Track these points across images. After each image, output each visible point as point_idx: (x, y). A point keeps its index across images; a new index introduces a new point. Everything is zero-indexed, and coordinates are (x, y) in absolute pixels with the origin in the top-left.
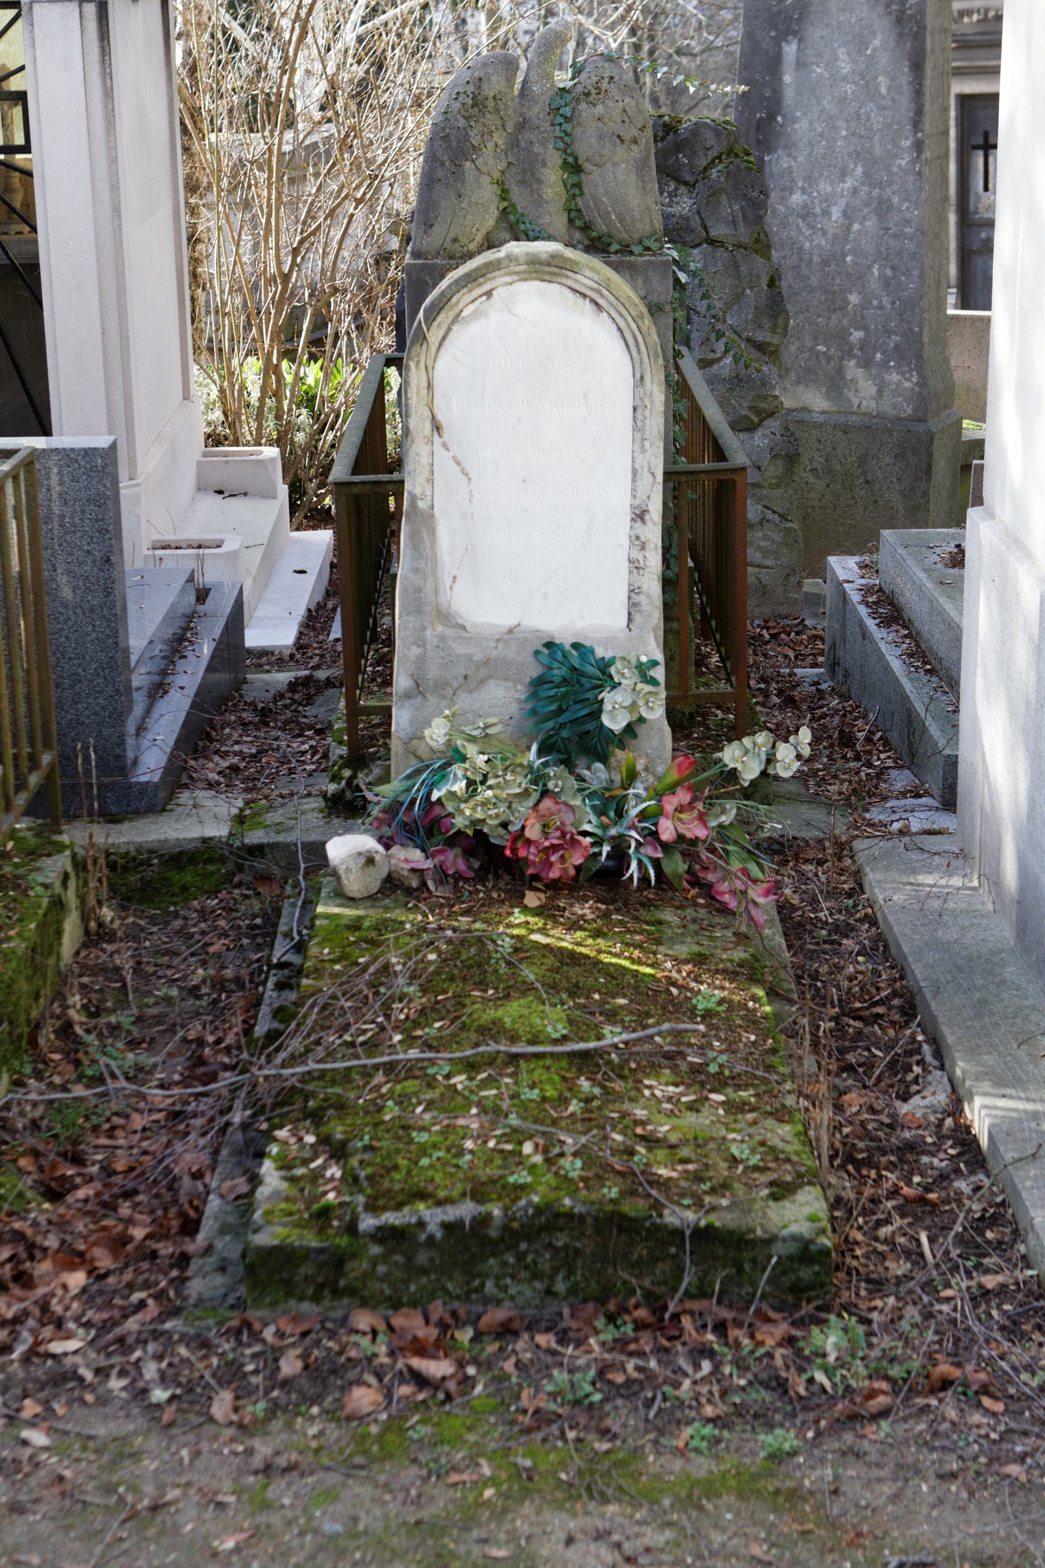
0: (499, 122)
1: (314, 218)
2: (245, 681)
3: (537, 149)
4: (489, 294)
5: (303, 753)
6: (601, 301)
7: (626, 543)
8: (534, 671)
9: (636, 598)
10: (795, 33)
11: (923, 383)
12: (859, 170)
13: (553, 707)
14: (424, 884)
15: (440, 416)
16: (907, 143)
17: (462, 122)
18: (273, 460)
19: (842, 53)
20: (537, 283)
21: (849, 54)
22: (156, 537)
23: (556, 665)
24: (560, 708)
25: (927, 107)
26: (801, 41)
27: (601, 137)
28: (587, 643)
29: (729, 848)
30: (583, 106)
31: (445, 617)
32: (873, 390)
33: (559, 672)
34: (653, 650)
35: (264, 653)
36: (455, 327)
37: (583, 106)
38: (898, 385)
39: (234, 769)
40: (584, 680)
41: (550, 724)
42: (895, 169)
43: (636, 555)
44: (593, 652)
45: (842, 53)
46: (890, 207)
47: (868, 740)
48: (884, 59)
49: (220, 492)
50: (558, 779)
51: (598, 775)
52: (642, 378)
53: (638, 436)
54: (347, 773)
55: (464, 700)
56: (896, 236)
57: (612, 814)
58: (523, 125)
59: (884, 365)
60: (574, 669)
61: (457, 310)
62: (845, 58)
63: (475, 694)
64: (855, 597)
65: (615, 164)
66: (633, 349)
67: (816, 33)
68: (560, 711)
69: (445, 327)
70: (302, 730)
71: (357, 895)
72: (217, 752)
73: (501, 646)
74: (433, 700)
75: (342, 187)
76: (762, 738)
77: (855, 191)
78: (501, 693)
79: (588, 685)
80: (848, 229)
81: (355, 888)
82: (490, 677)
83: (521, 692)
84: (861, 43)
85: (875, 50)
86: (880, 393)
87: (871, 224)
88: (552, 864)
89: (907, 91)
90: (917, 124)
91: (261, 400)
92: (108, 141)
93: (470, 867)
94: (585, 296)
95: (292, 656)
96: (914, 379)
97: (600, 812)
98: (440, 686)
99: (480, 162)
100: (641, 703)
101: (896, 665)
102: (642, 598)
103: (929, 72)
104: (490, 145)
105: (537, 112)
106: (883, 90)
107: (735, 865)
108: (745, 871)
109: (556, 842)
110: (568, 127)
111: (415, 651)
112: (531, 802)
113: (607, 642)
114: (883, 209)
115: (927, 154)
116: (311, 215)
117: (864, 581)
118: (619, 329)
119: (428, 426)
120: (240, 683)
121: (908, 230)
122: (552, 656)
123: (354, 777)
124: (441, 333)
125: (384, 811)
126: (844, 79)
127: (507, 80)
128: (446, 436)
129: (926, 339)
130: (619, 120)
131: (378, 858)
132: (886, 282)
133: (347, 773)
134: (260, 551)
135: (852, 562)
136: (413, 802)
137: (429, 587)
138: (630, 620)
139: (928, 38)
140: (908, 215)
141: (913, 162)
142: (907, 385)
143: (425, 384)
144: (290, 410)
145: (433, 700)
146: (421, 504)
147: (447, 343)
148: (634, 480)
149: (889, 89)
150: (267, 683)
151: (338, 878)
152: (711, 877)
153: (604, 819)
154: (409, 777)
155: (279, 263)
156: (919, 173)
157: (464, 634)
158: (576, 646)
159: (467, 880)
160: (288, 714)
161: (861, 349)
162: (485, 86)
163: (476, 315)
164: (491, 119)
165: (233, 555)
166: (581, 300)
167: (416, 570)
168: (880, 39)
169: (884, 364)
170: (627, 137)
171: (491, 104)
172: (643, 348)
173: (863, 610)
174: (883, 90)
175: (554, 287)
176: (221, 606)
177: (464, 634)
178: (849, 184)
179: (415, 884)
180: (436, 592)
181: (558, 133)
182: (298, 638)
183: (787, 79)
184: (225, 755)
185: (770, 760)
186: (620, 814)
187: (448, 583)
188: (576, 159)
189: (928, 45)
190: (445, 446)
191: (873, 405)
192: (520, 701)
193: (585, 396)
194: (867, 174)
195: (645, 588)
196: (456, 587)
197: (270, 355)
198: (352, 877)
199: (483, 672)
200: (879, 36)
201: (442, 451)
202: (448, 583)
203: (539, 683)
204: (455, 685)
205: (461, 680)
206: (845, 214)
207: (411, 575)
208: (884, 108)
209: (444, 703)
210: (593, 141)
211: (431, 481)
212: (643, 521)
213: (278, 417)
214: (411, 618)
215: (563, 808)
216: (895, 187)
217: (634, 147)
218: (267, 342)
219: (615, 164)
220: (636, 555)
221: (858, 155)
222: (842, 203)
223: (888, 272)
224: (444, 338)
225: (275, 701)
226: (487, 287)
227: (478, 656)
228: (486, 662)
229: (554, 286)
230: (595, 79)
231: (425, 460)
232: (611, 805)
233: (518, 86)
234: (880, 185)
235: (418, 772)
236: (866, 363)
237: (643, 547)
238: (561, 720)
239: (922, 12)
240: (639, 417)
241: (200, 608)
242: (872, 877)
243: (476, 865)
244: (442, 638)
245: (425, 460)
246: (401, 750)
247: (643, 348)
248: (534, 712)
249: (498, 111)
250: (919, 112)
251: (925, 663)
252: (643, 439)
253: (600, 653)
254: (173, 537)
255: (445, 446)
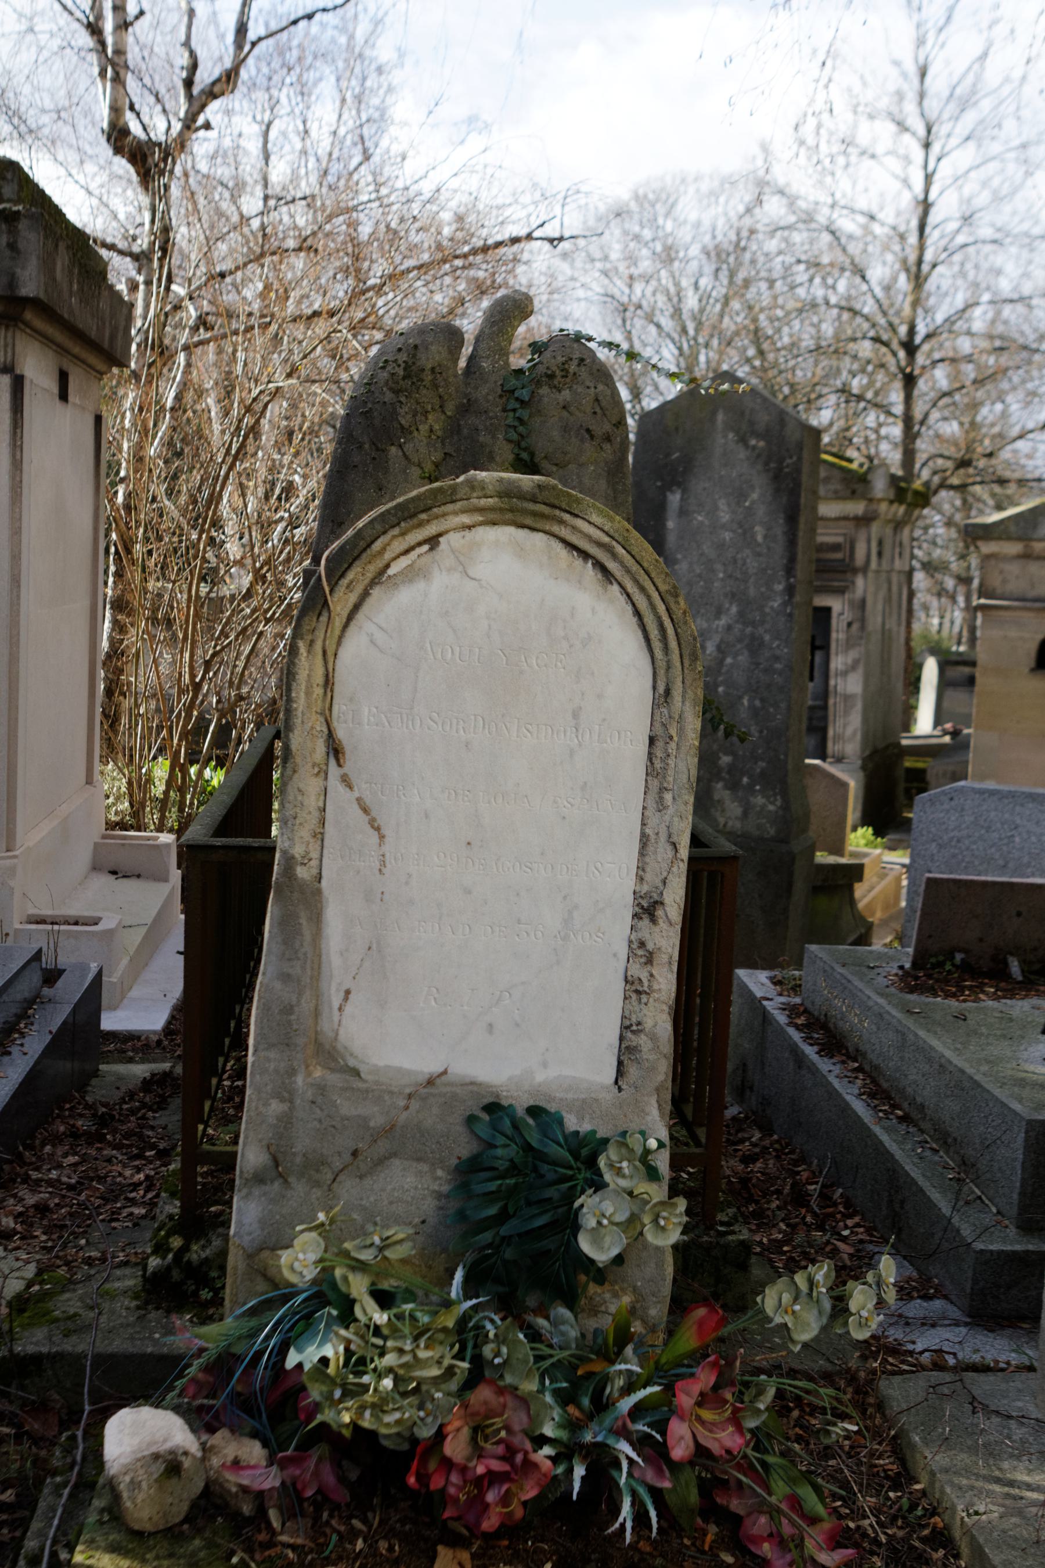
0: (436, 401)
1: (227, 637)
2: (96, 1073)
3: (482, 438)
4: (433, 542)
5: (135, 1186)
6: (611, 565)
7: (623, 951)
8: (464, 1148)
9: (632, 1039)
10: (679, 485)
11: (786, 807)
12: (734, 609)
13: (492, 1211)
14: (261, 1512)
15: (341, 733)
16: (779, 587)
17: (389, 396)
18: (167, 846)
19: (722, 504)
20: (511, 530)
21: (729, 505)
22: (32, 911)
23: (501, 1140)
24: (504, 1210)
25: (800, 556)
26: (684, 491)
27: (565, 429)
28: (552, 1108)
29: (771, 1459)
30: (544, 390)
31: (329, 1054)
32: (739, 811)
33: (505, 1153)
34: (655, 1128)
35: (130, 1037)
36: (376, 592)
37: (544, 390)
38: (763, 807)
39: (42, 1209)
40: (545, 1168)
41: (487, 1237)
42: (767, 610)
43: (637, 970)
44: (560, 1122)
45: (722, 504)
46: (762, 644)
47: (825, 1197)
48: (761, 511)
49: (114, 873)
50: (501, 1341)
51: (564, 1326)
52: (668, 692)
53: (655, 784)
54: (176, 1242)
55: (348, 1190)
56: (766, 671)
57: (586, 1402)
58: (467, 407)
59: (750, 788)
60: (528, 1148)
61: (380, 564)
62: (725, 508)
63: (368, 1182)
64: (782, 1018)
65: (581, 465)
66: (657, 645)
67: (699, 485)
68: (503, 1216)
69: (359, 589)
70: (143, 1150)
71: (149, 1527)
72: (26, 1179)
73: (415, 1105)
74: (299, 1188)
75: (254, 611)
76: (822, 1273)
77: (729, 628)
78: (410, 1180)
79: (550, 1176)
80: (721, 662)
81: (145, 1514)
82: (394, 1155)
83: (441, 1181)
84: (741, 495)
85: (753, 503)
86: (745, 814)
87: (743, 658)
88: (487, 1506)
89: (781, 538)
90: (790, 569)
91: (166, 793)
92: (13, 511)
93: (342, 1480)
94: (585, 555)
95: (159, 1042)
96: (779, 803)
97: (565, 1398)
98: (313, 1164)
99: (409, 448)
100: (647, 1219)
101: (859, 1107)
102: (643, 1041)
103: (802, 526)
104: (424, 428)
105: (485, 393)
106: (759, 538)
107: (780, 1488)
108: (795, 1502)
109: (496, 1465)
110: (524, 414)
111: (276, 1107)
112: (453, 1386)
113: (584, 1107)
114: (755, 646)
115: (797, 598)
116: (224, 634)
117: (782, 999)
118: (637, 613)
119: (321, 748)
120: (84, 1079)
121: (778, 666)
122: (494, 1126)
123: (185, 1249)
124: (353, 598)
125: (207, 1369)
126: (724, 527)
127: (450, 352)
128: (349, 767)
129: (790, 767)
130: (589, 410)
131: (187, 1463)
132: (755, 712)
133: (176, 1242)
134: (143, 931)
135: (763, 976)
136: (259, 1354)
137: (306, 1005)
138: (620, 1072)
139: (803, 495)
140: (778, 652)
141: (785, 604)
142: (771, 808)
143: (319, 679)
144: (192, 803)
145: (299, 1188)
146: (301, 872)
147: (360, 616)
148: (642, 853)
149: (765, 537)
150: (120, 1078)
151: (116, 1497)
152: (736, 1505)
153: (571, 1409)
154: (253, 1312)
155: (193, 676)
156: (790, 615)
157: (358, 1084)
158: (534, 1111)
159: (335, 1508)
160: (132, 1124)
161: (729, 772)
162: (422, 356)
163: (411, 575)
164: (426, 396)
165: (110, 933)
166: (579, 562)
167: (286, 978)
168: (759, 494)
169: (750, 788)
170: (598, 430)
171: (428, 377)
172: (673, 644)
173: (796, 1036)
174: (759, 538)
175: (539, 539)
176: (69, 992)
177: (358, 1084)
178: (723, 622)
179: (247, 1509)
180: (317, 1014)
181: (510, 421)
182: (169, 1023)
183: (670, 524)
184: (35, 1186)
185: (840, 1308)
186: (601, 1405)
187: (336, 1001)
188: (532, 455)
189: (803, 501)
190: (346, 780)
191: (738, 824)
192: (439, 1196)
193: (576, 715)
194: (741, 614)
195: (648, 1024)
196: (348, 1008)
197: (178, 752)
198: (140, 1497)
199: (383, 1147)
200: (758, 490)
201: (341, 788)
202: (336, 1001)
203: (470, 1169)
204: (338, 1164)
205: (347, 1157)
206: (719, 648)
207: (278, 985)
208: (759, 555)
209: (316, 1193)
210: (555, 434)
211: (320, 836)
212: (653, 920)
213: (181, 810)
214: (272, 1054)
215: (509, 1400)
216: (767, 626)
217: (607, 446)
218: (175, 741)
219: (581, 465)
220: (637, 970)
221: (733, 595)
222: (717, 638)
223: (757, 703)
224: (357, 607)
225: (123, 1101)
226: (431, 530)
227: (378, 1121)
228: (389, 1130)
229: (539, 538)
230: (560, 359)
231: (312, 802)
232: (582, 1387)
233: (462, 363)
234: (753, 624)
235: (267, 1306)
236: (733, 786)
237: (649, 960)
238: (504, 1231)
239: (798, 471)
240: (659, 753)
241: (46, 991)
242: (933, 1459)
243: (353, 1475)
244: (321, 1088)
245: (312, 802)
246: (242, 1266)
247: (673, 644)
248: (461, 1215)
249: (436, 387)
250: (792, 560)
251: (895, 1107)
252: (662, 789)
253: (572, 1123)
254: (49, 912)
255: (346, 780)
